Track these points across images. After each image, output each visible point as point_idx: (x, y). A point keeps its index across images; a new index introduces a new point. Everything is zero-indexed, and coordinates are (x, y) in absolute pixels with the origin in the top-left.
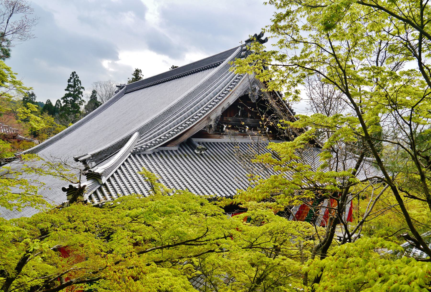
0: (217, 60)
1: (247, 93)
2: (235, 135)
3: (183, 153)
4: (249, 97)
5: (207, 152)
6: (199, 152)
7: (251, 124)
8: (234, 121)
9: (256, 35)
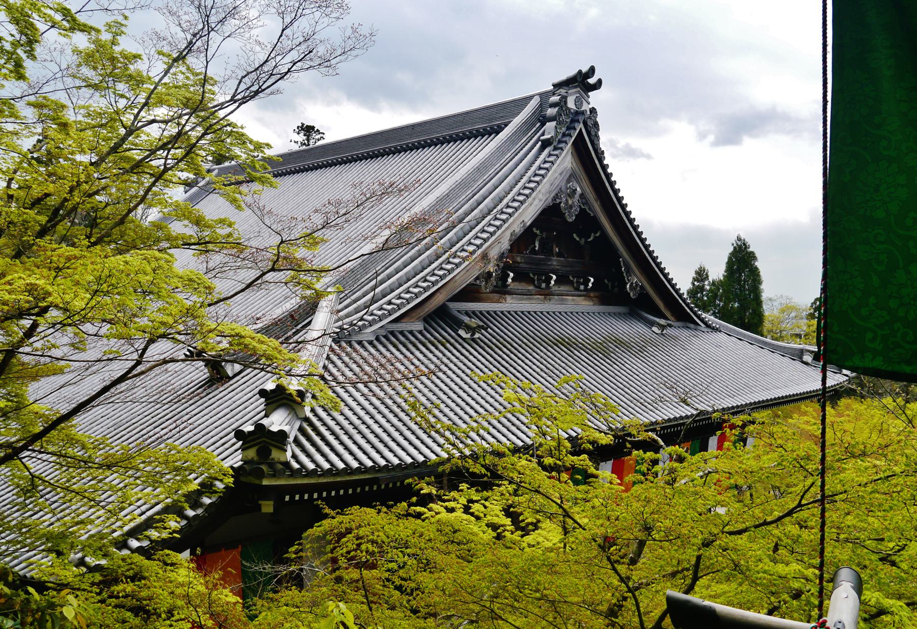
0: (479, 122)
1: (558, 201)
2: (527, 294)
3: (426, 338)
6: (468, 336)
7: (558, 270)
8: (525, 263)
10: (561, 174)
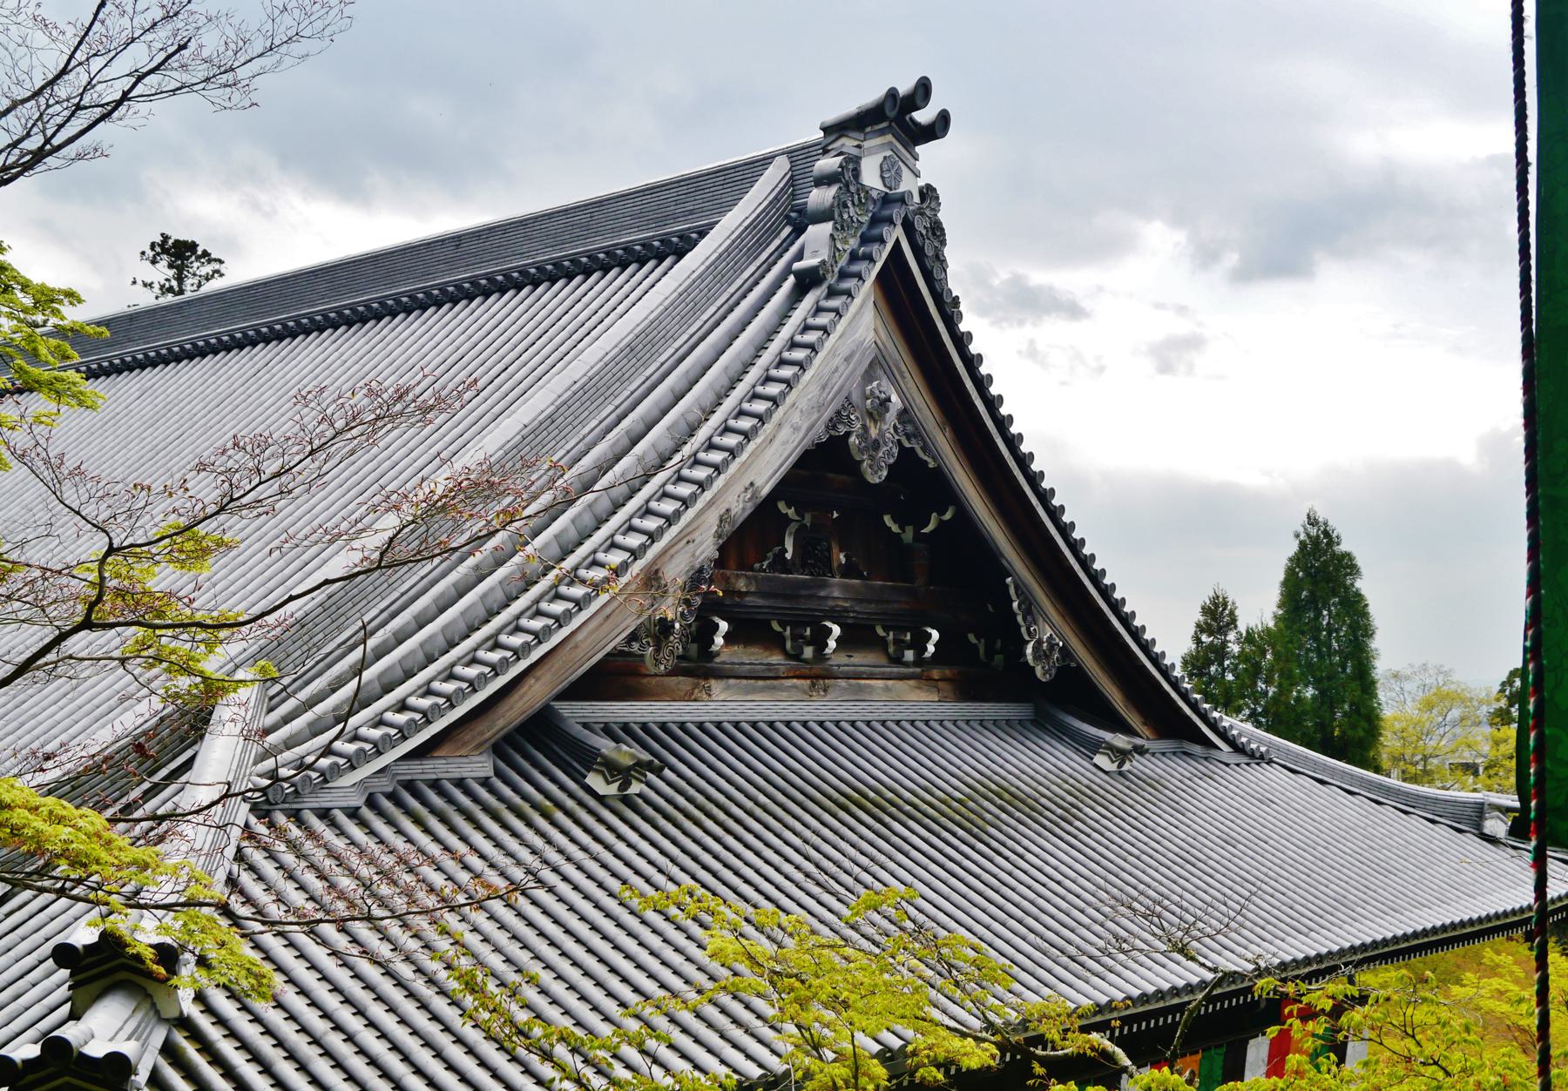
1: (842, 429)
3: (501, 798)
4: (854, 452)
5: (649, 785)
6: (612, 790)
7: (846, 610)
9: (892, 93)
10: (847, 360)
